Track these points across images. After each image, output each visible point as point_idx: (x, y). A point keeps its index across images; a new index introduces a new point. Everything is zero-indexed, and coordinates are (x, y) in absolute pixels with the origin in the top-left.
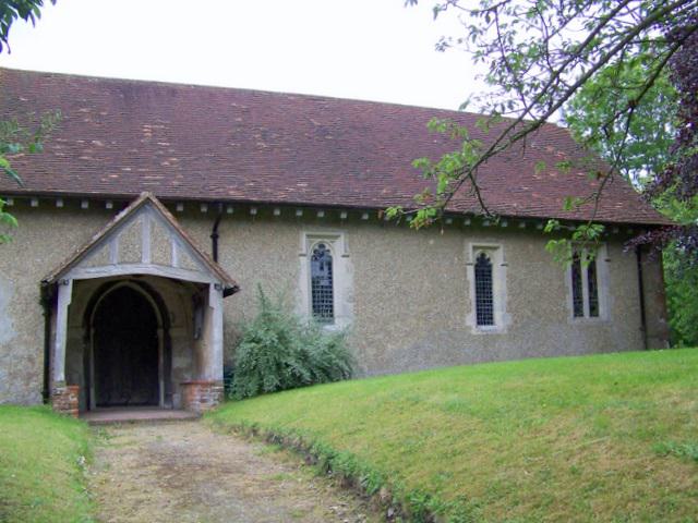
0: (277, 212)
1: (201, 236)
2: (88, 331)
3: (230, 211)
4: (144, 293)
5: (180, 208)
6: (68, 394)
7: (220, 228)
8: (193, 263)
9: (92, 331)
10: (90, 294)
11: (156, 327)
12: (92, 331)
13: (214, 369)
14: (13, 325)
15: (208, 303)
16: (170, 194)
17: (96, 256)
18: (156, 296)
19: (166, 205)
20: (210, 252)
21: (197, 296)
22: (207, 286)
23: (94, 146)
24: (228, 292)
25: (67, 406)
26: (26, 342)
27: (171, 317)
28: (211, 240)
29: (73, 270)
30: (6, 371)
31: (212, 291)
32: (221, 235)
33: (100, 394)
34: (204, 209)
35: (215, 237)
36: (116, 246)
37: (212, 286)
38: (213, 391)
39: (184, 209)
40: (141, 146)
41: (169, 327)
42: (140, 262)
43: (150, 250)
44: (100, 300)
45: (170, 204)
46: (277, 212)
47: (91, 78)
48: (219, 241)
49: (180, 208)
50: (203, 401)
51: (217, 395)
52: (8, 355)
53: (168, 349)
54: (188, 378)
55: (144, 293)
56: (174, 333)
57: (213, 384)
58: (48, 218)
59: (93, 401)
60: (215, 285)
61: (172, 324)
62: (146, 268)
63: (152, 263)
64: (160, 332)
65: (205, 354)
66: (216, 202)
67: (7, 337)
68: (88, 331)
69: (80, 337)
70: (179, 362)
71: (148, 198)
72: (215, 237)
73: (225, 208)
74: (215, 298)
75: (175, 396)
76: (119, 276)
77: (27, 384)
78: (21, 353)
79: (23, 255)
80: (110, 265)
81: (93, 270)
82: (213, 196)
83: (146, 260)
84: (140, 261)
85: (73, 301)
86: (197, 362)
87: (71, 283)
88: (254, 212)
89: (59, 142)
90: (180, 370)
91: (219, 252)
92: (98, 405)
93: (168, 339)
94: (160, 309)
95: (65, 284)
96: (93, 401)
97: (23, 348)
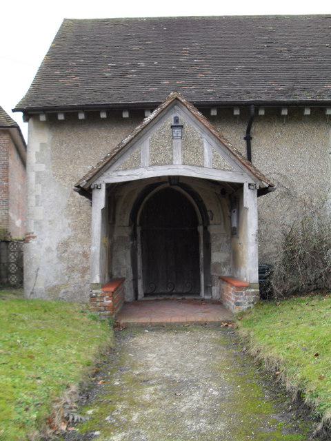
0: (307, 112)
1: (235, 137)
2: (135, 229)
3: (262, 113)
4: (183, 192)
5: (214, 113)
6: (102, 297)
7: (252, 130)
8: (225, 162)
9: (139, 230)
10: (135, 197)
11: (197, 224)
12: (139, 230)
13: (250, 271)
14: (69, 225)
15: (242, 203)
16: (203, 99)
17: (127, 158)
18: (194, 195)
19: (200, 110)
20: (244, 154)
21: (230, 194)
22: (241, 186)
23: (138, 67)
24: (262, 192)
25: (102, 308)
26: (80, 240)
27: (209, 214)
28: (244, 142)
29: (106, 174)
30: (65, 265)
31: (246, 190)
32: (254, 137)
33: (147, 284)
34: (237, 112)
35: (248, 139)
36: (145, 149)
37: (246, 186)
38: (247, 294)
39: (219, 113)
40: (179, 64)
41: (208, 224)
42: (172, 164)
43: (182, 153)
44: (145, 200)
45: (204, 108)
46: (307, 112)
47: (140, 18)
48: (253, 143)
49: (214, 113)
50: (238, 304)
51: (252, 298)
52: (66, 251)
53: (208, 247)
54: (226, 272)
55: (183, 192)
56: (213, 229)
57: (249, 287)
58: (95, 130)
59: (141, 292)
60: (249, 184)
61: (211, 222)
62: (178, 168)
63: (184, 164)
64: (200, 229)
65: (241, 253)
66: (248, 105)
67: (65, 236)
68: (135, 229)
69: (126, 235)
70: (217, 257)
71: (177, 99)
72: (248, 139)
73: (257, 111)
74: (249, 199)
75: (213, 288)
76: (159, 178)
77: (83, 277)
78: (77, 249)
79: (75, 163)
80: (144, 166)
81: (125, 173)
82: (246, 99)
83: (178, 160)
84: (171, 163)
85: (106, 205)
86: (235, 259)
87: (104, 187)
88: (285, 112)
89: (109, 67)
90: (218, 264)
91: (253, 153)
92: (146, 295)
93: (207, 235)
94: (137, 213)
95: (98, 188)
96: (141, 292)
97: (78, 245)
